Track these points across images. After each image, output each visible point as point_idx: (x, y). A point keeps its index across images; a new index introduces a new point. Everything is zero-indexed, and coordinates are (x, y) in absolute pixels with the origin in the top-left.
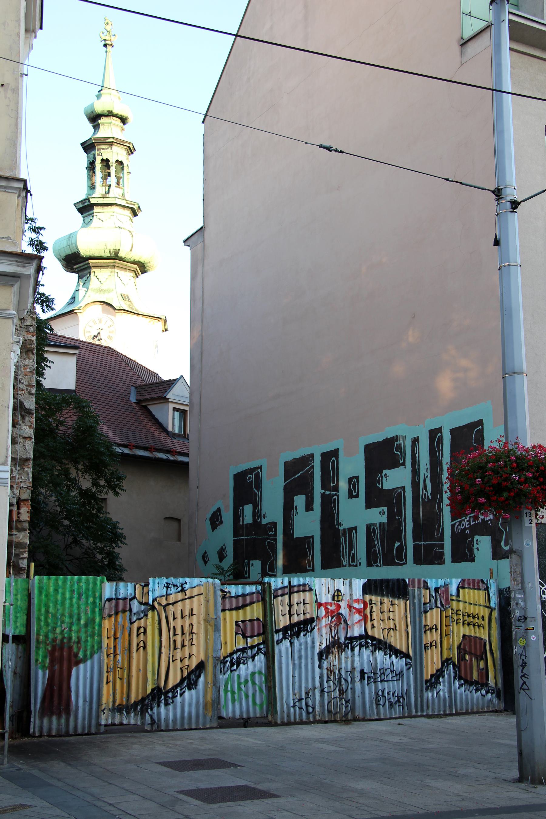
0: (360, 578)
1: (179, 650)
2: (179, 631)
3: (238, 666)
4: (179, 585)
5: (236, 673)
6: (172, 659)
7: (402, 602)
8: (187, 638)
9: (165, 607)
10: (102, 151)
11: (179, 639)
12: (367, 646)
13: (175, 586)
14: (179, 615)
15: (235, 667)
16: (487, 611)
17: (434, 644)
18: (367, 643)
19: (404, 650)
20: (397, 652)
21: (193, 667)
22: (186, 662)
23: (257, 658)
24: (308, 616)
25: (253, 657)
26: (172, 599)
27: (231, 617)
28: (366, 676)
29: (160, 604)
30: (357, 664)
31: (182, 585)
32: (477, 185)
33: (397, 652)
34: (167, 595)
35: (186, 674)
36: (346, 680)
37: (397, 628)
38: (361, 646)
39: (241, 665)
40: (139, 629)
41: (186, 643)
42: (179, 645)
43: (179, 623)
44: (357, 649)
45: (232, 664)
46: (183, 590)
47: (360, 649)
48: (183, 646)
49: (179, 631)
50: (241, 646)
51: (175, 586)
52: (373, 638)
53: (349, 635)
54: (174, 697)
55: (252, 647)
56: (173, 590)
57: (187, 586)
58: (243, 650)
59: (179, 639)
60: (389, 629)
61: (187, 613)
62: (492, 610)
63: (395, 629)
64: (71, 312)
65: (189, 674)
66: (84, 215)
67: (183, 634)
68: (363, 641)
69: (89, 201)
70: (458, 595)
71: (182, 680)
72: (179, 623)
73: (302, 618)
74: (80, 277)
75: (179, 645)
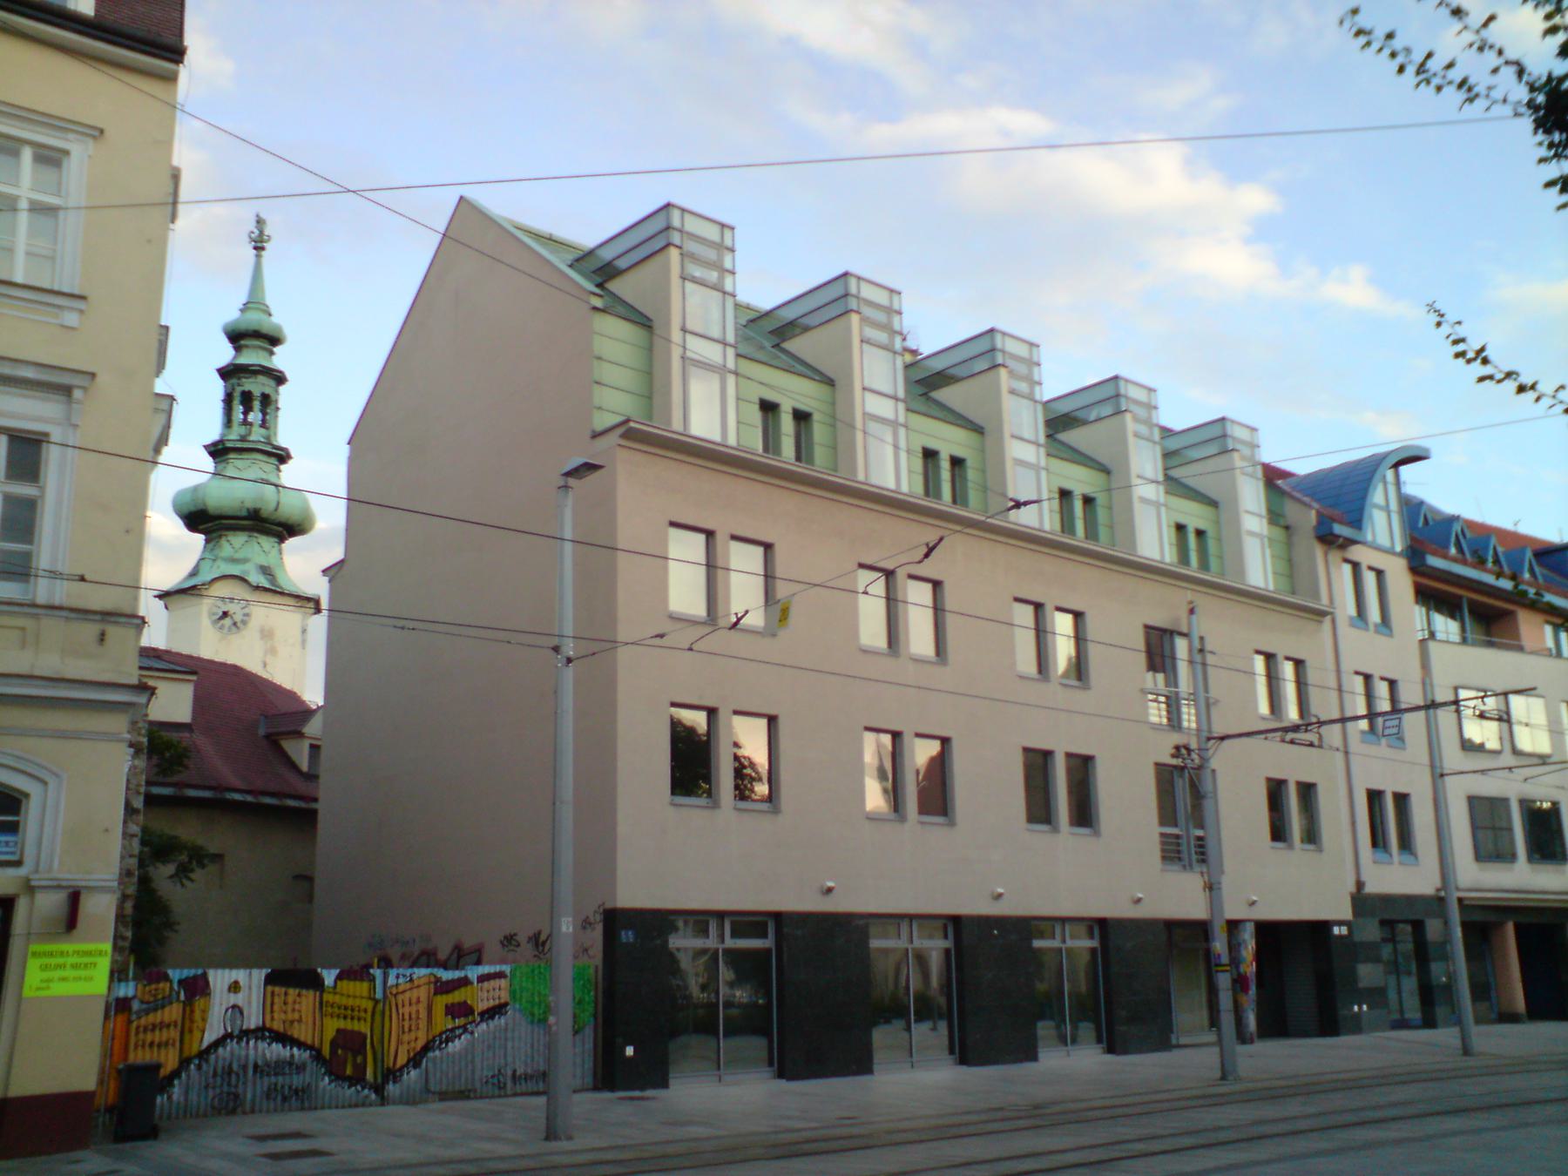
0: (260, 967)
1: (407, 1034)
2: (407, 1017)
3: (447, 1045)
4: (408, 975)
5: (445, 1051)
6: (399, 1042)
7: (311, 993)
8: (414, 1023)
9: (395, 995)
10: (244, 380)
11: (406, 1024)
12: (263, 1038)
13: (404, 976)
14: (407, 1003)
15: (444, 1045)
16: (370, 1005)
17: (171, 1041)
18: (263, 1035)
19: (309, 1042)
20: (300, 1044)
21: (419, 1049)
22: (413, 1044)
23: (463, 1037)
24: (502, 1001)
25: (460, 1036)
26: (401, 988)
27: (442, 1001)
28: (259, 1070)
29: (391, 993)
30: (252, 1058)
31: (411, 975)
32: (166, 466)
33: (300, 1044)
34: (397, 985)
35: (412, 1054)
36: (238, 1075)
37: (304, 1020)
38: (257, 1039)
39: (450, 1044)
40: (138, 1027)
41: (413, 1028)
42: (406, 1029)
43: (407, 1010)
44: (252, 1043)
45: (441, 1043)
46: (411, 980)
47: (256, 1042)
48: (410, 1030)
49: (407, 1017)
50: (450, 1027)
51: (404, 976)
52: (270, 1030)
53: (244, 1027)
54: (402, 1075)
55: (459, 1027)
56: (401, 980)
57: (415, 977)
58: (452, 1030)
59: (406, 1024)
60: (292, 1022)
61: (414, 1001)
62: (376, 1002)
63: (300, 1021)
64: (194, 587)
65: (415, 1055)
66: (217, 460)
67: (410, 1018)
68: (260, 1034)
69: (224, 444)
70: (335, 987)
71: (409, 1061)
72: (407, 1010)
73: (497, 1002)
74: (207, 541)
75: (406, 1029)
